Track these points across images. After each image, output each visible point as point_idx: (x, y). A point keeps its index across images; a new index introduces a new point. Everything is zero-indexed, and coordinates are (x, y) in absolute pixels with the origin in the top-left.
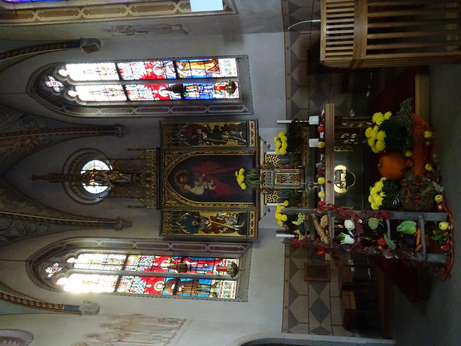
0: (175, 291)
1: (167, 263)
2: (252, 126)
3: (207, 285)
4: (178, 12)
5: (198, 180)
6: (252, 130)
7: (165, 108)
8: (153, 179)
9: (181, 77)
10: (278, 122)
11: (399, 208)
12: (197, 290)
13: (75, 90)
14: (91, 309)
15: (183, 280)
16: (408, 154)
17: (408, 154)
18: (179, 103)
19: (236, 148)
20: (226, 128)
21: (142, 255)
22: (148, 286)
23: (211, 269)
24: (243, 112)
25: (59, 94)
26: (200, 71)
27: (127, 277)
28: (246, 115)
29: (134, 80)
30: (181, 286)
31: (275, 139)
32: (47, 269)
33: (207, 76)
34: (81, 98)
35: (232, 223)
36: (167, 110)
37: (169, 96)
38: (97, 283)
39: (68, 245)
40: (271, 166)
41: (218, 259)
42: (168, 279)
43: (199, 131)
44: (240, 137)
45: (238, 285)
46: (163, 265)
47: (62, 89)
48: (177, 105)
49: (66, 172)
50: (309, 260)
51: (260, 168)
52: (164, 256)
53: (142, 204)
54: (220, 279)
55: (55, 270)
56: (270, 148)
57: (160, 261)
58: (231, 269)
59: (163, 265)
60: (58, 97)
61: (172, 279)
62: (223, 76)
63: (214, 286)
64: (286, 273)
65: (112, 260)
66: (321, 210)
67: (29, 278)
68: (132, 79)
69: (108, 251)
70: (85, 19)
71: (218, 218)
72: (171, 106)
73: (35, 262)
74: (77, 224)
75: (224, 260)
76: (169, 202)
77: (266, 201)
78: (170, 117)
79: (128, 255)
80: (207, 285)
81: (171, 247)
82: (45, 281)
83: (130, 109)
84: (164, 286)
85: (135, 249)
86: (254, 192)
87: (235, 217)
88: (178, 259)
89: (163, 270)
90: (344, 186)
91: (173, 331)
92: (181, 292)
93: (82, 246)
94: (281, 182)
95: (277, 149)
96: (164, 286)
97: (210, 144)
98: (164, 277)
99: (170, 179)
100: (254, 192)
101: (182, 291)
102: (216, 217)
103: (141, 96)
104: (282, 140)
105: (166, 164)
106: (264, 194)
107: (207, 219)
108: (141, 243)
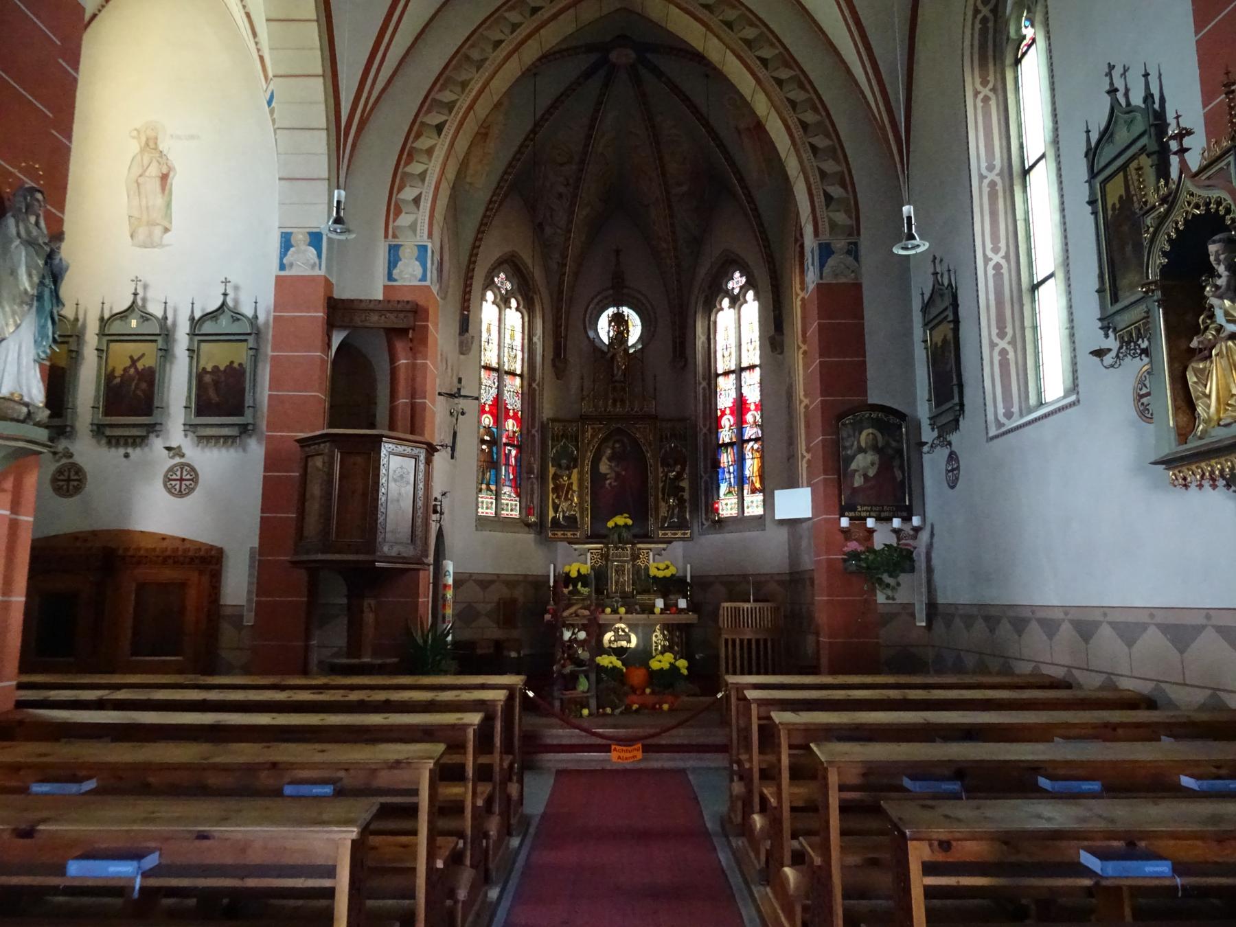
0: (483, 442)
2: (684, 534)
6: (679, 534)
7: (708, 423)
8: (618, 409)
9: (745, 446)
11: (599, 680)
13: (730, 307)
15: (494, 449)
16: (648, 691)
17: (648, 691)
18: (714, 441)
19: (657, 513)
21: (522, 394)
23: (507, 483)
24: (702, 522)
25: (724, 286)
26: (751, 469)
29: (741, 386)
31: (668, 563)
34: (720, 314)
35: (565, 509)
36: (705, 425)
37: (722, 428)
38: (488, 343)
39: (532, 299)
40: (635, 557)
42: (495, 430)
43: (678, 468)
44: (672, 518)
46: (510, 422)
47: (730, 292)
49: (625, 291)
51: (633, 544)
54: (496, 495)
56: (657, 556)
57: (515, 417)
59: (510, 422)
63: (489, 489)
65: (515, 357)
66: (594, 610)
70: (798, 351)
73: (513, 261)
74: (559, 310)
75: (518, 499)
79: (521, 376)
85: (530, 385)
86: (605, 537)
87: (573, 513)
88: (518, 441)
90: (612, 645)
94: (616, 570)
95: (655, 565)
99: (619, 430)
100: (605, 537)
102: (572, 489)
103: (723, 392)
105: (637, 426)
106: (601, 549)
107: (569, 478)
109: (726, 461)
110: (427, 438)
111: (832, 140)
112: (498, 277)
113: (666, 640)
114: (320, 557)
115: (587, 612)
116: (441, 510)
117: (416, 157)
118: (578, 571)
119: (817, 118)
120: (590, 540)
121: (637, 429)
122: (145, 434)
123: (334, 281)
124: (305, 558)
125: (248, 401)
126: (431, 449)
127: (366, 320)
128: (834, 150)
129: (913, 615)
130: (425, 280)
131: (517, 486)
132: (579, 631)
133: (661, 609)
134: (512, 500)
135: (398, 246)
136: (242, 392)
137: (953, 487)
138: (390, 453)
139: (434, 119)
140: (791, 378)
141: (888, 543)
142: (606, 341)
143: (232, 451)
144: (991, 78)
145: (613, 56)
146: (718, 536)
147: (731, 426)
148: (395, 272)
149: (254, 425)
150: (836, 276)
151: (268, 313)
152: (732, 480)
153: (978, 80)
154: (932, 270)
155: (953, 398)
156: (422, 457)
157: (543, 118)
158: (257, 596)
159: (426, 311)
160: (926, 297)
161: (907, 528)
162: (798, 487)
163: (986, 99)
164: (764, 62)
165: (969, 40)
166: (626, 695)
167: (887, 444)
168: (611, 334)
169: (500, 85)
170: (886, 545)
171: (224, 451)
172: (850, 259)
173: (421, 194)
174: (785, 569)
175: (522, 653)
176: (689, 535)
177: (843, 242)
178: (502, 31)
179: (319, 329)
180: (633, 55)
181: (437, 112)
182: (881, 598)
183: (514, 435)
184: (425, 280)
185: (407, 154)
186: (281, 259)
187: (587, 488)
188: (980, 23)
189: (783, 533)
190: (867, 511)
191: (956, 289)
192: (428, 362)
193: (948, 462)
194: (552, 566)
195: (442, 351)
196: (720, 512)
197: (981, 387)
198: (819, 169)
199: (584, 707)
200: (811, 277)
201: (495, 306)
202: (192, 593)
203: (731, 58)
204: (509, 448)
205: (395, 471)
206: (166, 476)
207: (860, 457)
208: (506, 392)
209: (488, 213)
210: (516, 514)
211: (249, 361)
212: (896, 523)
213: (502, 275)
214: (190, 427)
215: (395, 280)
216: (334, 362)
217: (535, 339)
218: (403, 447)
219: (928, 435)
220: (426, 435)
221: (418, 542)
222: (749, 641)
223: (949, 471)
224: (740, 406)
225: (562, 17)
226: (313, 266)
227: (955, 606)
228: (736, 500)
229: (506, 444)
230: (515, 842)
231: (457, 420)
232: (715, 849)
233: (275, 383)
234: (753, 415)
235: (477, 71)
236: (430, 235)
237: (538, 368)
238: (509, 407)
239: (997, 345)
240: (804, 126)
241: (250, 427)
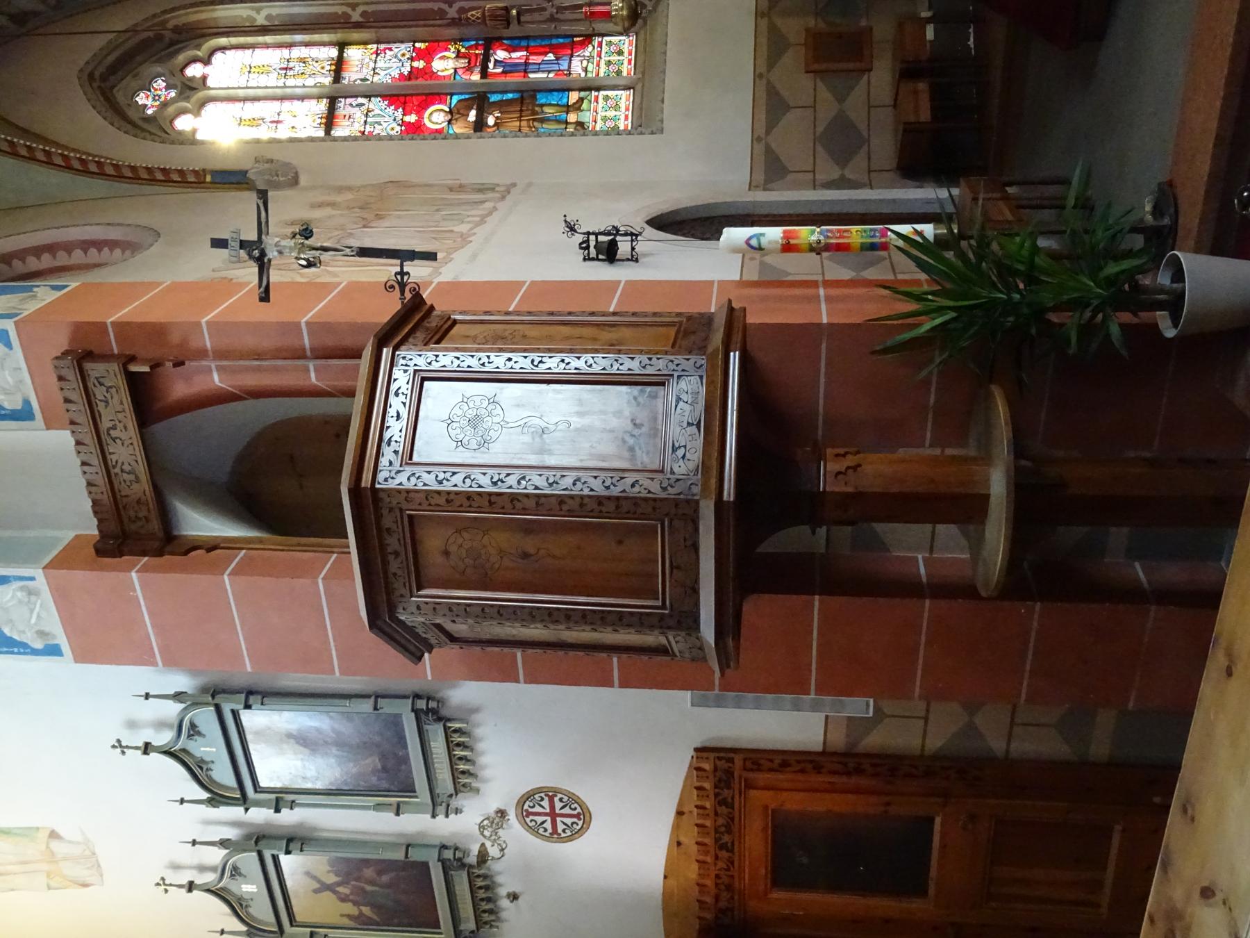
0: (479, 125)
1: (448, 58)
3: (557, 105)
12: (534, 120)
14: (278, 176)
15: (494, 98)
21: (378, 42)
22: (407, 119)
23: (564, 65)
27: (349, 100)
30: (491, 114)
32: (138, 95)
38: (278, 122)
39: (177, 30)
41: (581, 39)
42: (455, 99)
45: (638, 101)
50: (819, 20)
52: (438, 41)
54: (590, 89)
55: (159, 96)
57: (427, 55)
58: (622, 9)
61: (467, 97)
63: (577, 107)
64: (758, 62)
65: (303, 61)
67: (100, 117)
69: (287, 38)
73: (104, 78)
79: (342, 46)
80: (557, 105)
82: (145, 126)
84: (450, 117)
85: (358, 26)
88: (476, 46)
89: (441, 76)
91: (489, 205)
92: (494, 129)
96: (450, 117)
98: (447, 94)
101: (496, 124)
116: (609, 234)
122: (464, 874)
131: (571, 44)
134: (599, 55)
138: (408, 456)
143: (479, 732)
159: (79, 329)
175: (925, 14)
183: (464, 56)
186: (35, 652)
202: (794, 802)
204: (491, 65)
205: (460, 443)
206: (548, 839)
208: (376, 79)
213: (141, 99)
214: (439, 804)
217: (261, 20)
218: (390, 421)
229: (484, 73)
231: (326, 249)
238: (406, 70)
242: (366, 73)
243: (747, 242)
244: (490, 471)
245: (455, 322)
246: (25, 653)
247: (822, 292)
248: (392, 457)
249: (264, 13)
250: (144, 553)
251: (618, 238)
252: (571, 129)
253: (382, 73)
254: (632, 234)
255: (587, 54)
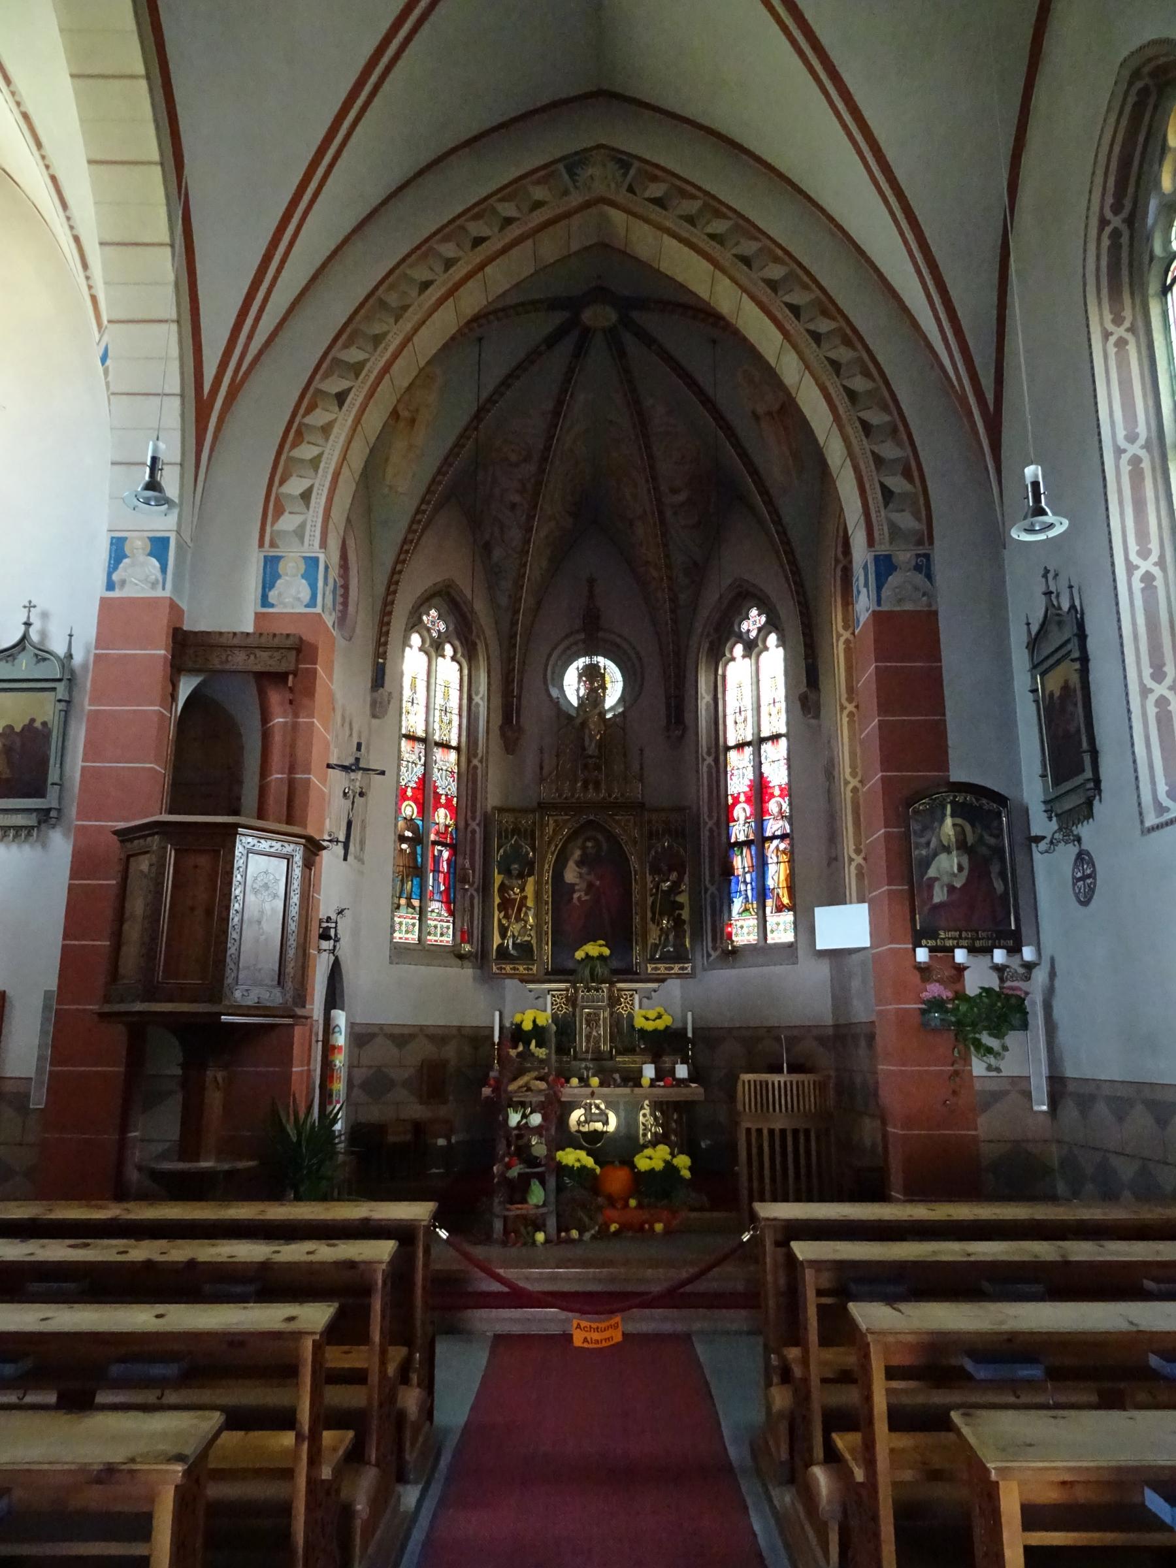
0: (402, 839)
2: (682, 969)
4: (851, 860)
5: (589, 874)
6: (676, 969)
7: (715, 815)
8: (591, 794)
9: (767, 845)
10: (690, 1014)
11: (560, 1188)
13: (744, 657)
15: (419, 849)
16: (633, 1203)
17: (633, 1203)
20: (678, 923)
23: (436, 897)
24: (707, 952)
25: (737, 629)
26: (776, 878)
27: (423, 751)
28: (703, 957)
29: (761, 763)
31: (661, 1010)
33: (767, 891)
34: (731, 664)
35: (516, 934)
36: (710, 817)
37: (735, 821)
38: (413, 703)
39: (474, 645)
40: (614, 1001)
42: (420, 823)
43: (674, 876)
45: (412, 947)
46: (442, 812)
47: (745, 637)
48: (719, 834)
49: (601, 634)
51: (612, 983)
52: (457, 814)
53: (545, 771)
54: (421, 914)
56: (645, 1000)
57: (447, 805)
59: (442, 812)
60: (732, 626)
62: (768, 919)
63: (409, 905)
65: (450, 722)
68: (763, 760)
69: (465, 714)
71: (524, 909)
72: (718, 824)
73: (448, 594)
75: (451, 919)
76: (551, 822)
77: (554, 993)
78: (699, 824)
79: (458, 749)
81: (473, 825)
83: (713, 750)
85: (469, 761)
87: (526, 938)
88: (452, 839)
93: (473, 669)
94: (586, 1020)
95: (643, 1012)
97: (651, 896)
100: (572, 972)
103: (735, 772)
104: (658, 1021)
106: (567, 990)
107: (523, 890)
108: (479, 772)
109: (740, 866)
110: (311, 831)
111: (890, 414)
112: (428, 615)
113: (658, 1125)
114: (139, 1007)
115: (542, 1085)
116: (336, 935)
117: (307, 437)
118: (534, 1021)
119: (870, 385)
120: (552, 977)
121: (617, 822)
123: (184, 605)
124: (123, 1007)
125: (53, 776)
126: (313, 848)
127: (227, 661)
128: (895, 431)
129: (1027, 1095)
130: (315, 606)
131: (449, 902)
132: (531, 1113)
133: (652, 1080)
134: (441, 921)
135: (278, 559)
136: (44, 763)
137: (1085, 903)
138: (249, 851)
139: (334, 385)
140: (831, 749)
141: (987, 986)
142: (575, 703)
143: (26, 848)
144: (1128, 313)
145: (587, 316)
146: (734, 972)
147: (747, 818)
148: (272, 595)
149: (59, 810)
150: (900, 601)
151: (88, 652)
152: (749, 893)
153: (1108, 317)
154: (1043, 589)
155: (1083, 771)
156: (298, 859)
157: (491, 400)
158: (51, 1065)
159: (314, 649)
160: (1035, 629)
161: (1015, 963)
162: (845, 903)
163: (1121, 343)
164: (795, 310)
165: (1094, 260)
166: (600, 1208)
167: (981, 840)
168: (582, 692)
169: (429, 341)
170: (982, 988)
171: (14, 848)
172: (919, 578)
173: (312, 487)
174: (829, 1021)
175: (453, 1141)
176: (689, 970)
177: (908, 555)
178: (432, 269)
179: (159, 673)
180: (613, 316)
181: (339, 376)
182: (978, 1067)
184: (315, 606)
185: (294, 433)
186: (109, 575)
187: (547, 903)
188: (1109, 238)
189: (823, 970)
190: (954, 939)
191: (1082, 614)
192: (315, 720)
193: (1075, 865)
194: (497, 1014)
195: (344, 710)
196: (734, 938)
197: (1129, 753)
198: (873, 453)
199: (538, 1228)
200: (864, 604)
201: (422, 653)
203: (749, 306)
204: (439, 848)
207: (943, 857)
208: (436, 770)
209: (415, 527)
210: (448, 940)
211: (56, 718)
212: (999, 956)
213: (433, 613)
215: (272, 606)
216: (182, 721)
217: (477, 699)
218: (269, 843)
219: (1041, 824)
220: (309, 826)
221: (289, 985)
222: (783, 1132)
223: (1079, 879)
224: (760, 790)
225: (514, 252)
226: (154, 585)
227: (1098, 1083)
228: (755, 922)
229: (435, 843)
230: (410, 1496)
231: (353, 803)
232: (746, 1508)
233: (92, 751)
234: (777, 802)
235: (396, 322)
236: (323, 544)
237: (480, 735)
238: (440, 791)
239: (1151, 691)
240: (852, 395)
241: (53, 814)
242: (440, 764)
243: (337, 1026)
244: (242, 895)
245: (311, 869)
246: (109, 567)
247: (306, 1068)
248: (252, 844)
249: (481, 702)
250: (173, 656)
251: (332, 942)
252: (396, 901)
253: (439, 775)
254: (334, 950)
255: (443, 912)
